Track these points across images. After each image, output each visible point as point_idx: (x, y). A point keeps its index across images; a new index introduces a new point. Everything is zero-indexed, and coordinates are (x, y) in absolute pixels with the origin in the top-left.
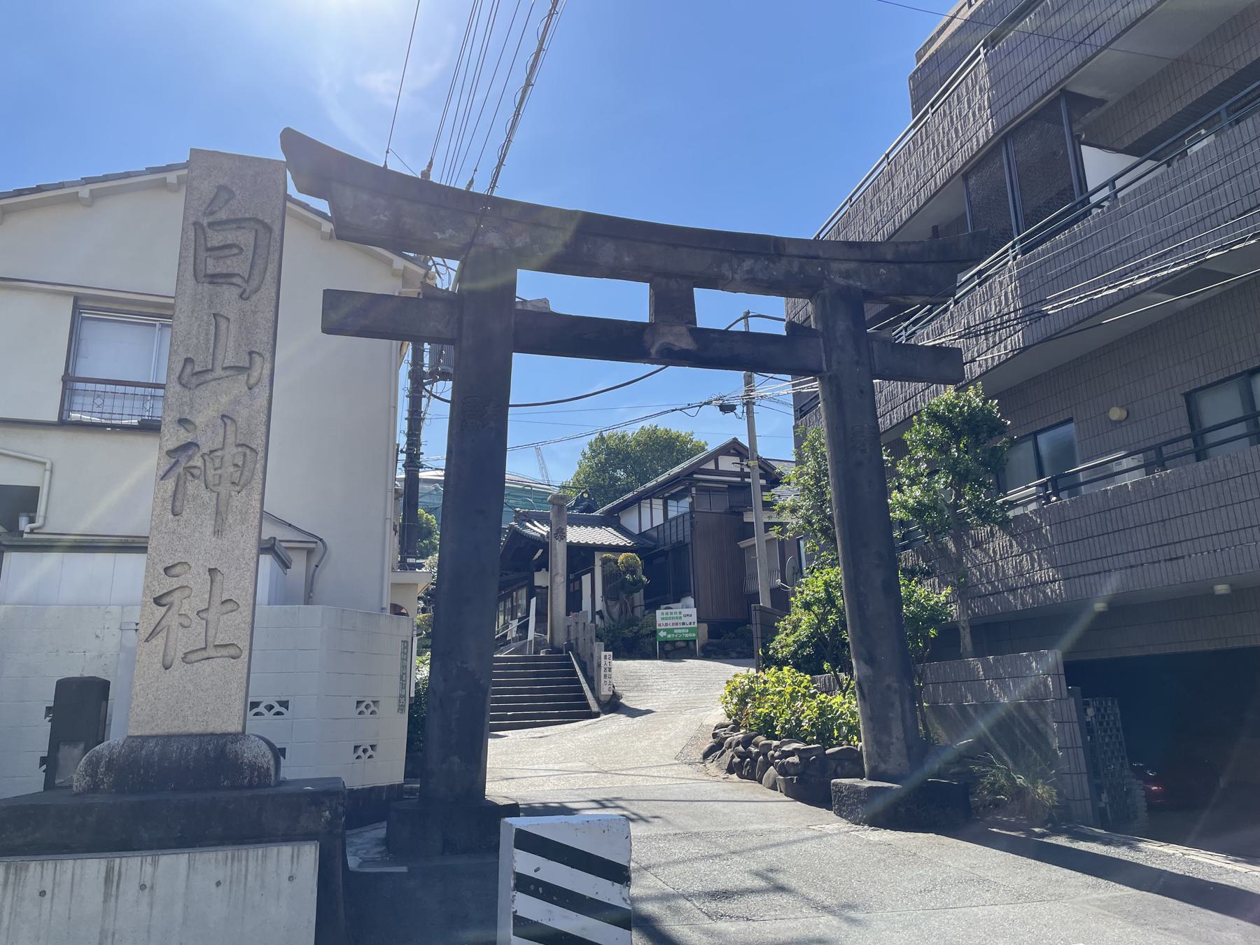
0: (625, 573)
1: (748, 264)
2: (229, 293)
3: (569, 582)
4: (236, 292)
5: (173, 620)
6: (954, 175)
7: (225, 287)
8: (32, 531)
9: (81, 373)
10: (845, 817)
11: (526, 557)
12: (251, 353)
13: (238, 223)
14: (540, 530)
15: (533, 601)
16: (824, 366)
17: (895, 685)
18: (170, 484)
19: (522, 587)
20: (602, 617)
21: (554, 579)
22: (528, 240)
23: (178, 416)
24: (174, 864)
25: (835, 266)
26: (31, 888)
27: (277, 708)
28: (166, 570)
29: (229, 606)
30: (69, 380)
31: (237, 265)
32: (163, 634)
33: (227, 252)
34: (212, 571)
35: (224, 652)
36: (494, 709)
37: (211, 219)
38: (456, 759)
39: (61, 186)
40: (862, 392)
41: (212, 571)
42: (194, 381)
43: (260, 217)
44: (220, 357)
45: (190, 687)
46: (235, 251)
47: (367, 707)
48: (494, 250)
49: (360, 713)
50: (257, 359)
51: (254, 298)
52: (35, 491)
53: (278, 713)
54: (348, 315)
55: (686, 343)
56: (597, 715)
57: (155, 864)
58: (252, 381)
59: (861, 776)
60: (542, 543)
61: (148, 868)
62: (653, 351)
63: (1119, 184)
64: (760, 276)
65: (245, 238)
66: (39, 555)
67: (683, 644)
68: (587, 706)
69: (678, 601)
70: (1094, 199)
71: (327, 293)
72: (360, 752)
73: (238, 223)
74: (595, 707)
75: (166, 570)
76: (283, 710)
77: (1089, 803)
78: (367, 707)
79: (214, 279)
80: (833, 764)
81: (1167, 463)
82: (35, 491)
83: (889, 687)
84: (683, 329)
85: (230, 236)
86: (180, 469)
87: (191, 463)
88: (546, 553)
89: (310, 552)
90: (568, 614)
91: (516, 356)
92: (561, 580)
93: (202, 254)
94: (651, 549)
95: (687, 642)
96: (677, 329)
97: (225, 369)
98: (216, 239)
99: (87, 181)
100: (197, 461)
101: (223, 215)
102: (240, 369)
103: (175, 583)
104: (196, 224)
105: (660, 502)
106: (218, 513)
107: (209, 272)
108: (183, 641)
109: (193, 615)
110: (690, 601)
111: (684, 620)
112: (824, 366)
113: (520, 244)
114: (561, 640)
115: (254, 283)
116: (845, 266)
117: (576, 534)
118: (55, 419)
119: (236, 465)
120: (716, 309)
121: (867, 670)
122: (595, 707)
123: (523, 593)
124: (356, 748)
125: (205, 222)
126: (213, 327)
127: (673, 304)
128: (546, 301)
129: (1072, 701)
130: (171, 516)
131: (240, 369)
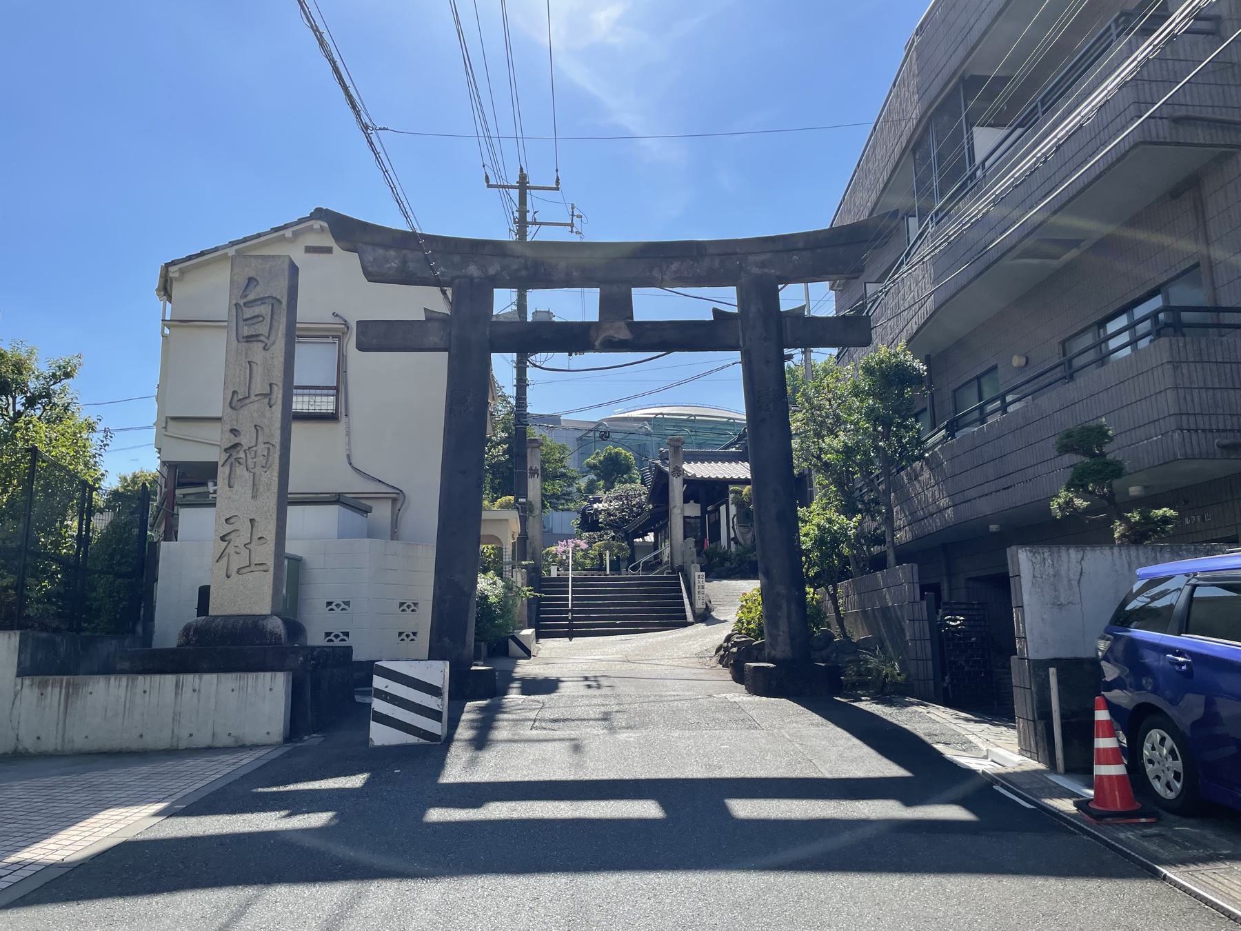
0: (749, 504)
1: (675, 266)
4: (261, 345)
12: (271, 385)
13: (262, 300)
17: (784, 592)
20: (736, 543)
24: (210, 679)
25: (751, 258)
26: (139, 689)
27: (343, 606)
28: (227, 520)
29: (262, 541)
31: (263, 329)
32: (226, 558)
33: (256, 320)
35: (261, 568)
38: (447, 640)
39: (216, 249)
40: (768, 362)
42: (239, 404)
48: (471, 279)
50: (275, 387)
55: (624, 334)
56: (691, 624)
57: (200, 679)
61: (197, 681)
62: (597, 343)
63: (987, 164)
65: (264, 310)
68: (685, 617)
72: (404, 636)
73: (262, 300)
74: (690, 618)
75: (227, 520)
77: (931, 684)
79: (249, 339)
80: (755, 653)
85: (257, 310)
86: (232, 460)
89: (394, 500)
90: (685, 538)
93: (241, 323)
96: (617, 324)
98: (248, 313)
99: (233, 244)
101: (251, 297)
104: (236, 305)
106: (254, 484)
115: (272, 338)
116: (763, 257)
120: (652, 304)
122: (690, 618)
124: (400, 634)
127: (616, 305)
129: (924, 603)
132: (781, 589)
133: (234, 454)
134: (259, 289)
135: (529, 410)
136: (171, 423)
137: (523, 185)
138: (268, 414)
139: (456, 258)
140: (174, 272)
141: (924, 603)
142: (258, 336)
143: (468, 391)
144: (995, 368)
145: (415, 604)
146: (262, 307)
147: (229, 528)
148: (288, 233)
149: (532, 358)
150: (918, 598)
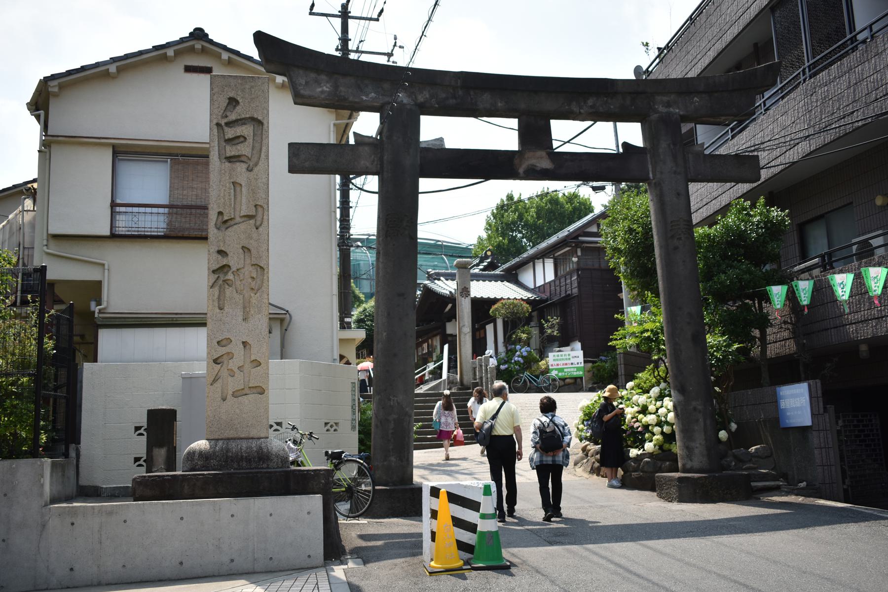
2: (241, 168)
3: (474, 331)
5: (224, 373)
6: (763, 9)
7: (238, 164)
8: (100, 312)
9: (118, 201)
10: (663, 498)
11: (438, 310)
12: (256, 206)
14: (446, 287)
15: (446, 347)
16: (651, 175)
18: (216, 290)
19: (435, 335)
21: (462, 326)
22: (428, 96)
23: (217, 249)
25: (658, 98)
27: (275, 427)
28: (218, 343)
30: (114, 205)
31: (244, 149)
34: (245, 344)
36: (417, 414)
37: (226, 120)
38: (393, 459)
41: (245, 344)
43: (255, 116)
44: (238, 209)
45: (238, 411)
46: (242, 139)
47: (331, 426)
49: (328, 430)
50: (260, 209)
51: (256, 170)
52: (99, 284)
53: (276, 430)
54: (305, 159)
55: (545, 164)
58: (258, 223)
59: (677, 471)
60: (451, 299)
62: (521, 171)
64: (601, 109)
65: (246, 130)
66: (124, 330)
67: (572, 381)
69: (567, 345)
70: (860, 37)
71: (291, 145)
75: (218, 343)
76: (279, 428)
78: (331, 426)
79: (230, 159)
81: (834, 264)
82: (99, 284)
83: (695, 409)
84: (543, 153)
85: (239, 130)
86: (220, 282)
87: (227, 278)
88: (454, 307)
91: (422, 117)
92: (467, 329)
94: (547, 300)
95: (575, 378)
97: (241, 217)
98: (230, 133)
100: (230, 276)
101: (233, 117)
102: (250, 217)
103: (223, 350)
105: (552, 261)
106: (244, 308)
107: (228, 155)
108: (233, 384)
109: (236, 370)
110: (578, 345)
111: (572, 360)
112: (651, 175)
113: (422, 100)
114: (468, 379)
115: (254, 160)
117: (481, 289)
118: (108, 233)
119: (253, 278)
121: (681, 398)
123: (437, 342)
125: (223, 122)
126: (232, 191)
127: (535, 134)
128: (441, 140)
130: (218, 311)
131: (250, 217)
132: (698, 404)
133: (222, 277)
134: (239, 109)
135: (352, 232)
136: (52, 243)
137: (344, 15)
138: (255, 236)
139: (386, 86)
140: (53, 86)
141: (827, 415)
142: (239, 156)
143: (399, 212)
144: (852, 203)
145: (336, 424)
146: (244, 127)
147: (222, 351)
148: (170, 52)
149: (353, 181)
150: (822, 411)
